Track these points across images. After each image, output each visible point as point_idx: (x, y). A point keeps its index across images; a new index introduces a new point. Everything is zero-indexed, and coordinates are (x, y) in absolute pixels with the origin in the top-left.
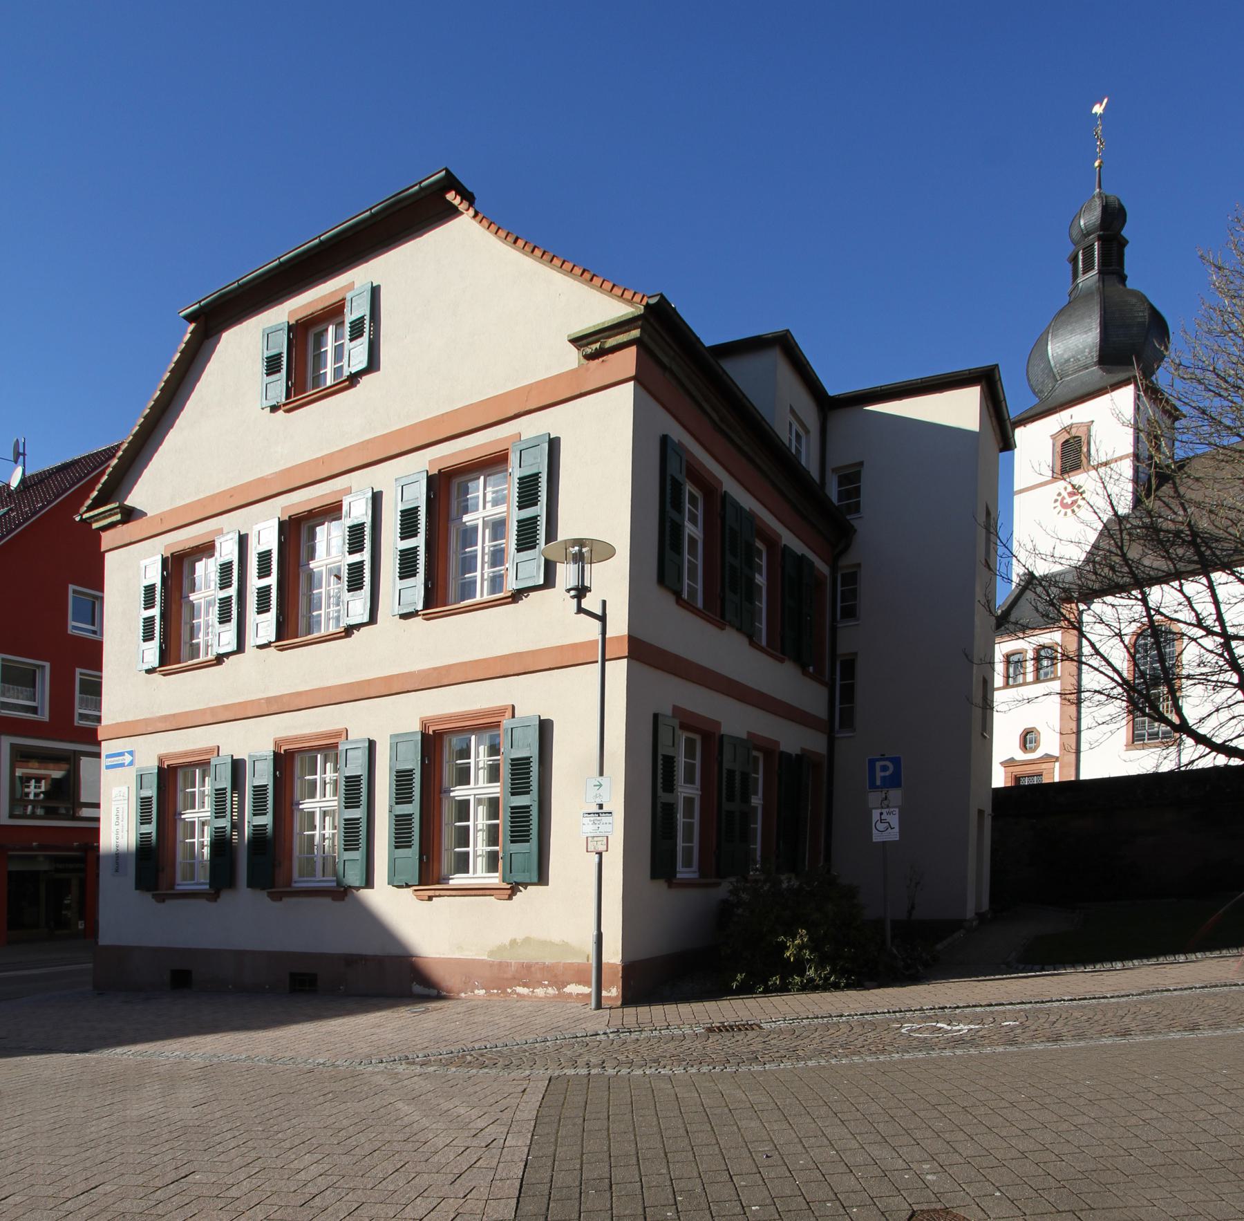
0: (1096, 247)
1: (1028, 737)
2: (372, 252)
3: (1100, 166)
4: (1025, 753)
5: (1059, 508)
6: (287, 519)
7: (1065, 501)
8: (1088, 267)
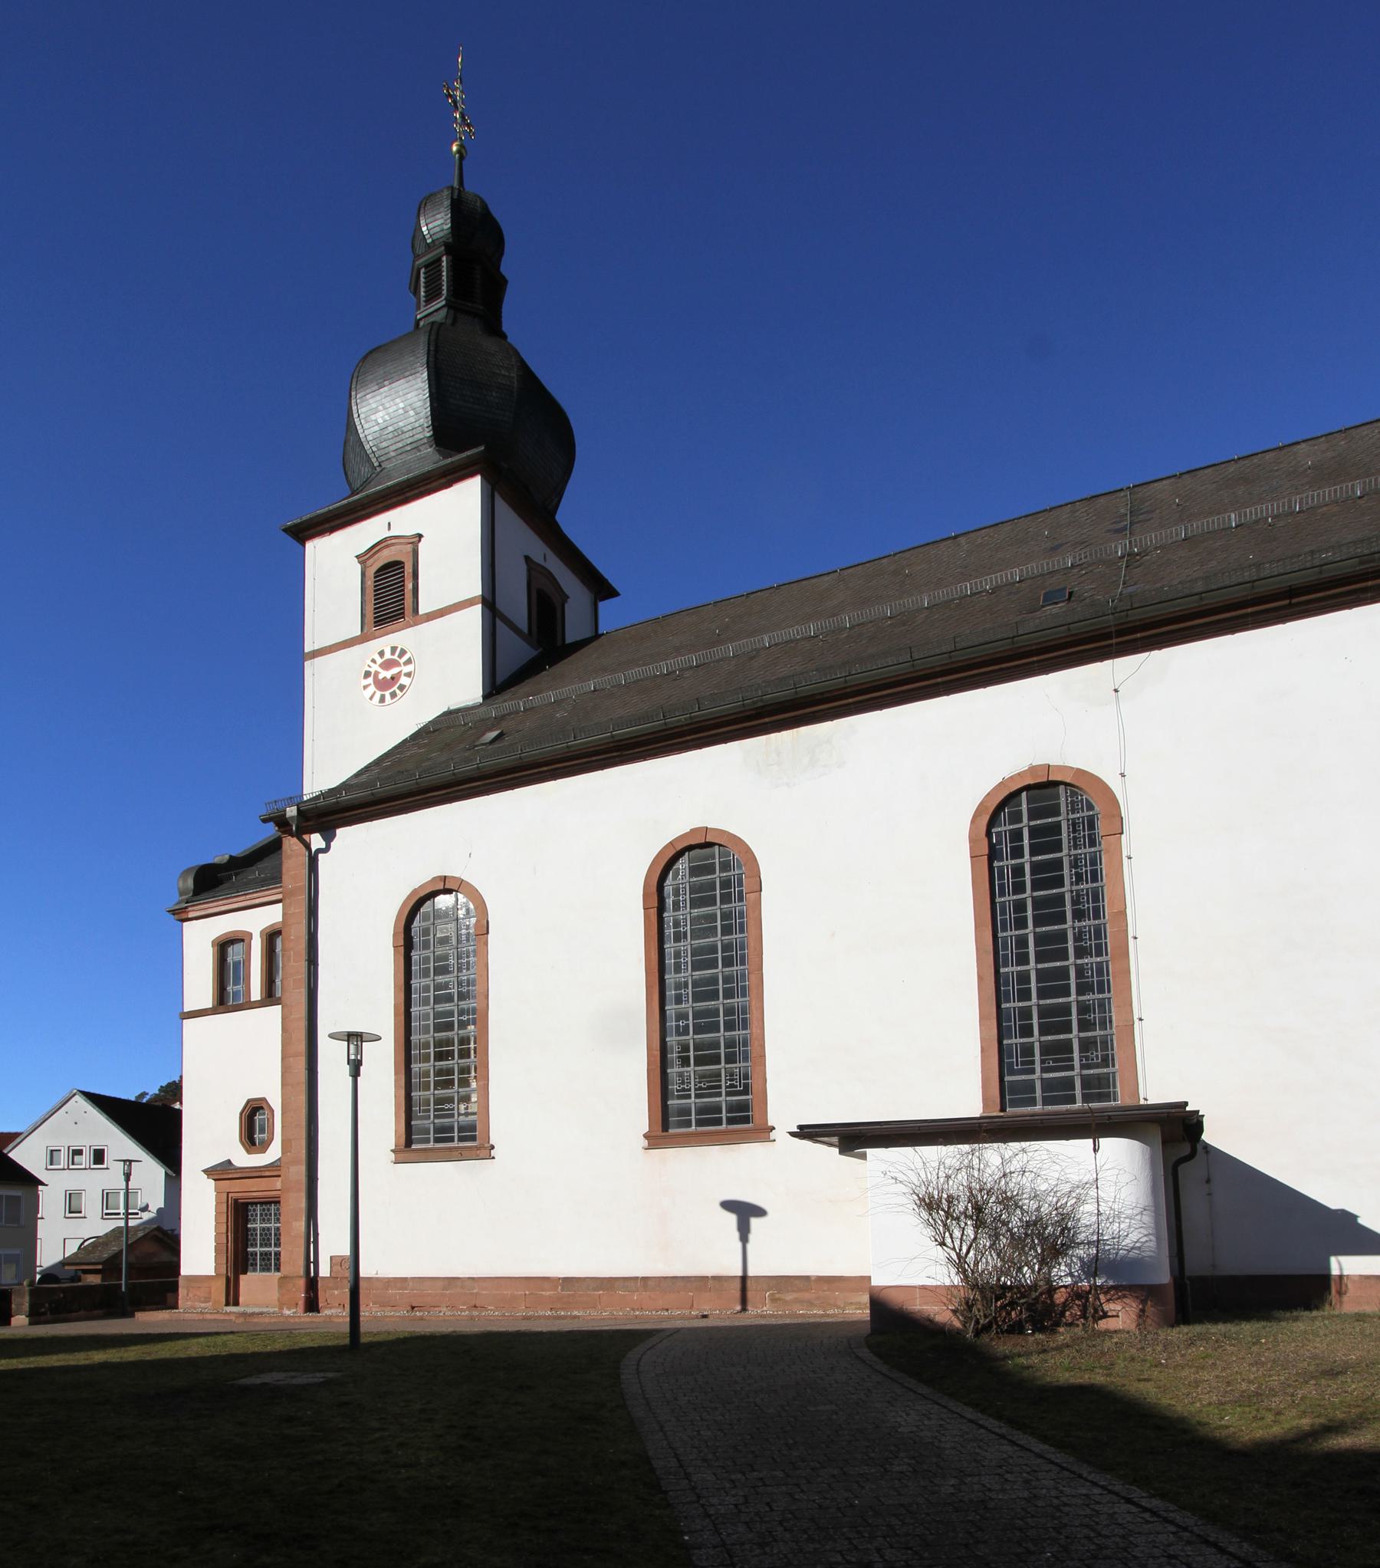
0: (444, 264)
3: (459, 151)
4: (249, 1152)
5: (372, 689)
6: (770, 1124)
7: (381, 677)
8: (433, 294)
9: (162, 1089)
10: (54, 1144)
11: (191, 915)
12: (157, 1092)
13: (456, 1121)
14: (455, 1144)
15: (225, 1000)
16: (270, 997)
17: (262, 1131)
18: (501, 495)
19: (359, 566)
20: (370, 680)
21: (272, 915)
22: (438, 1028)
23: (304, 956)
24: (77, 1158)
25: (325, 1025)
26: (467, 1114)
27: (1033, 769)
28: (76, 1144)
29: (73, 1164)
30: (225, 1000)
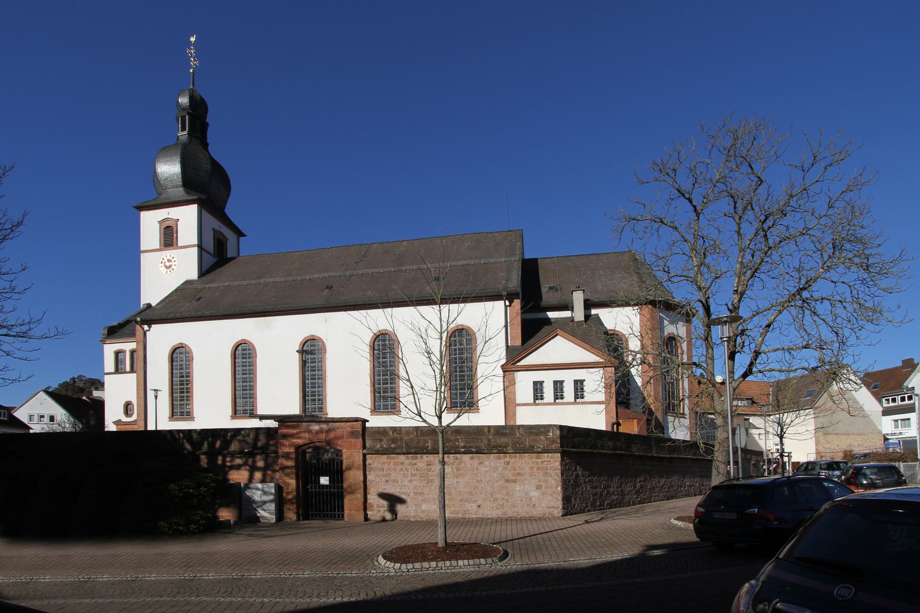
1: (129, 407)
2: (599, 307)
9: (60, 385)
10: (32, 412)
11: (107, 342)
12: (57, 387)
13: (185, 410)
14: (185, 417)
15: (118, 370)
16: (132, 370)
17: (130, 411)
18: (204, 209)
19: (159, 225)
20: (163, 265)
21: (133, 346)
22: (181, 385)
23: (142, 361)
24: (42, 419)
25: (149, 387)
26: (189, 409)
27: (311, 336)
28: (42, 413)
29: (40, 421)
30: (118, 370)
